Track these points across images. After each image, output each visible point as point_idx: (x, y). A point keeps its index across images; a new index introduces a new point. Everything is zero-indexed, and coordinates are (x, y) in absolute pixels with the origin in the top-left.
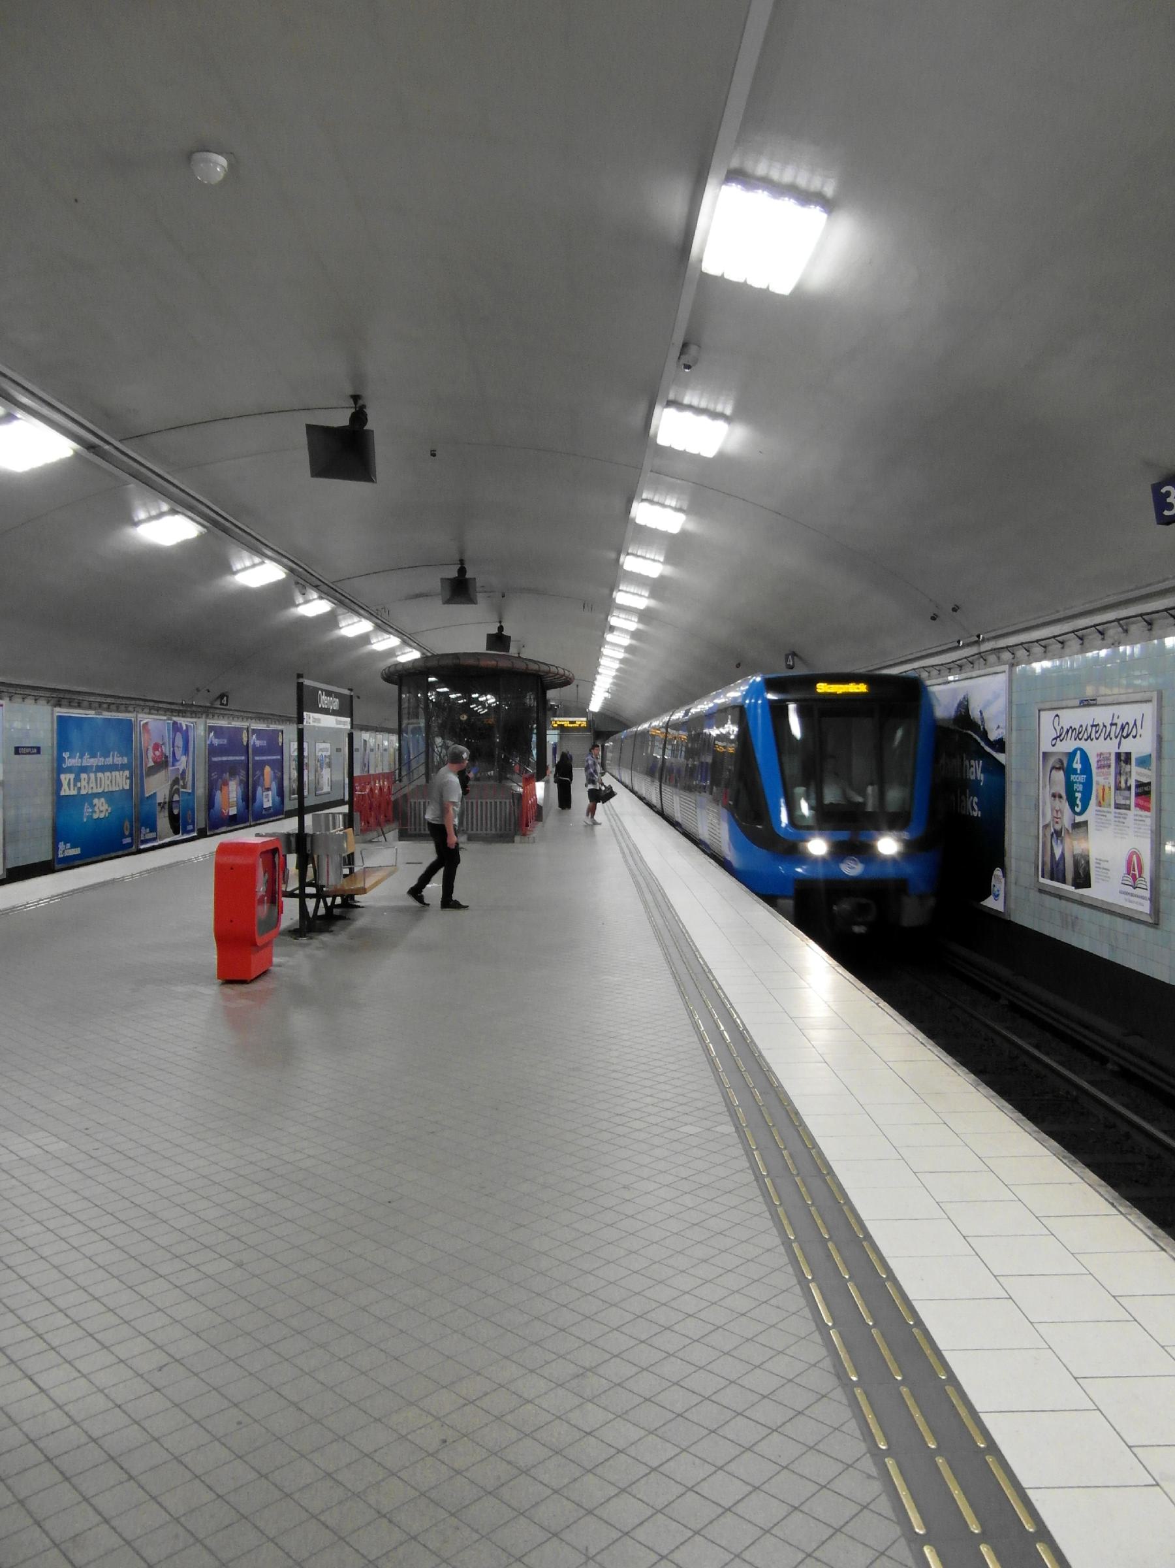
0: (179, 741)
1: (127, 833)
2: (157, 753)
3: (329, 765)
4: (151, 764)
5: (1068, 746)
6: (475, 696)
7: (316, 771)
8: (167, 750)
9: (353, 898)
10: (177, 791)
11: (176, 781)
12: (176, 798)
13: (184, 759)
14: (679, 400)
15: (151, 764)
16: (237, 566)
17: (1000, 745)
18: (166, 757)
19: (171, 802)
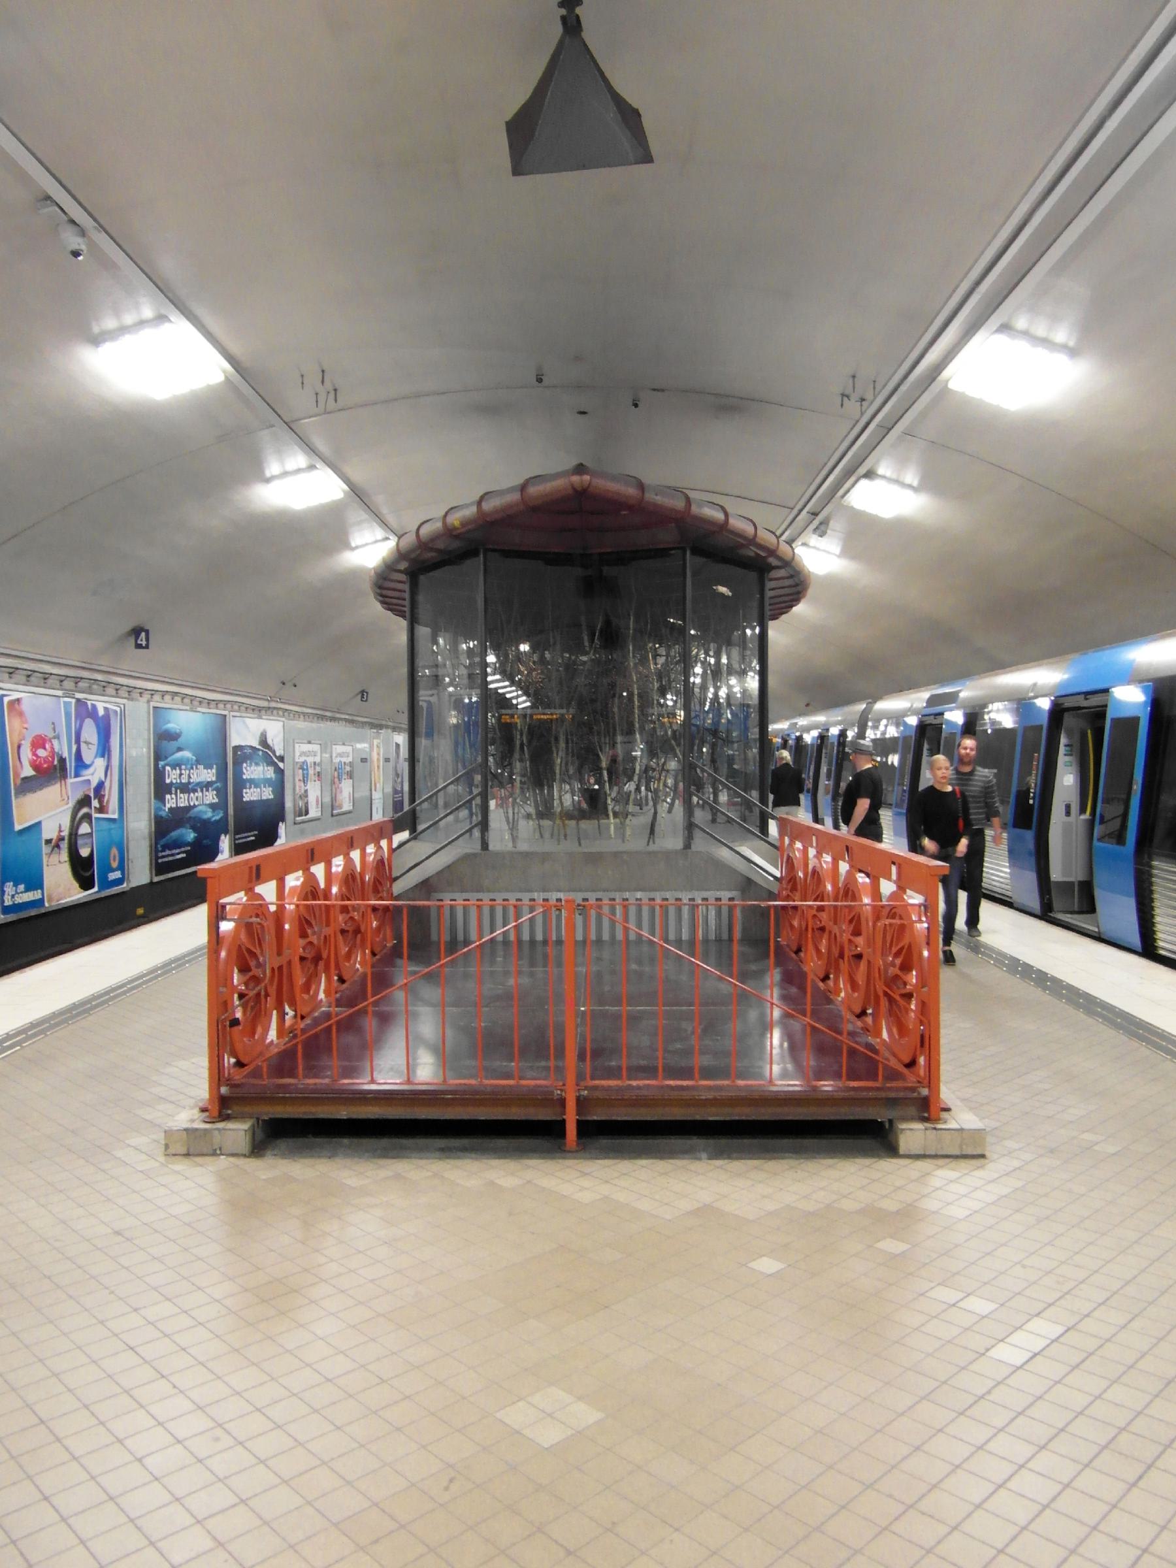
0: (90, 732)
1: (115, 865)
2: (42, 753)
3: (350, 775)
4: (28, 771)
5: (302, 759)
6: (491, 658)
7: (333, 783)
8: (64, 748)
9: (935, 751)
10: (88, 817)
11: (85, 801)
12: (84, 828)
13: (100, 763)
14: (901, 479)
15: (28, 771)
16: (273, 468)
17: (282, 759)
18: (62, 761)
19: (74, 835)
